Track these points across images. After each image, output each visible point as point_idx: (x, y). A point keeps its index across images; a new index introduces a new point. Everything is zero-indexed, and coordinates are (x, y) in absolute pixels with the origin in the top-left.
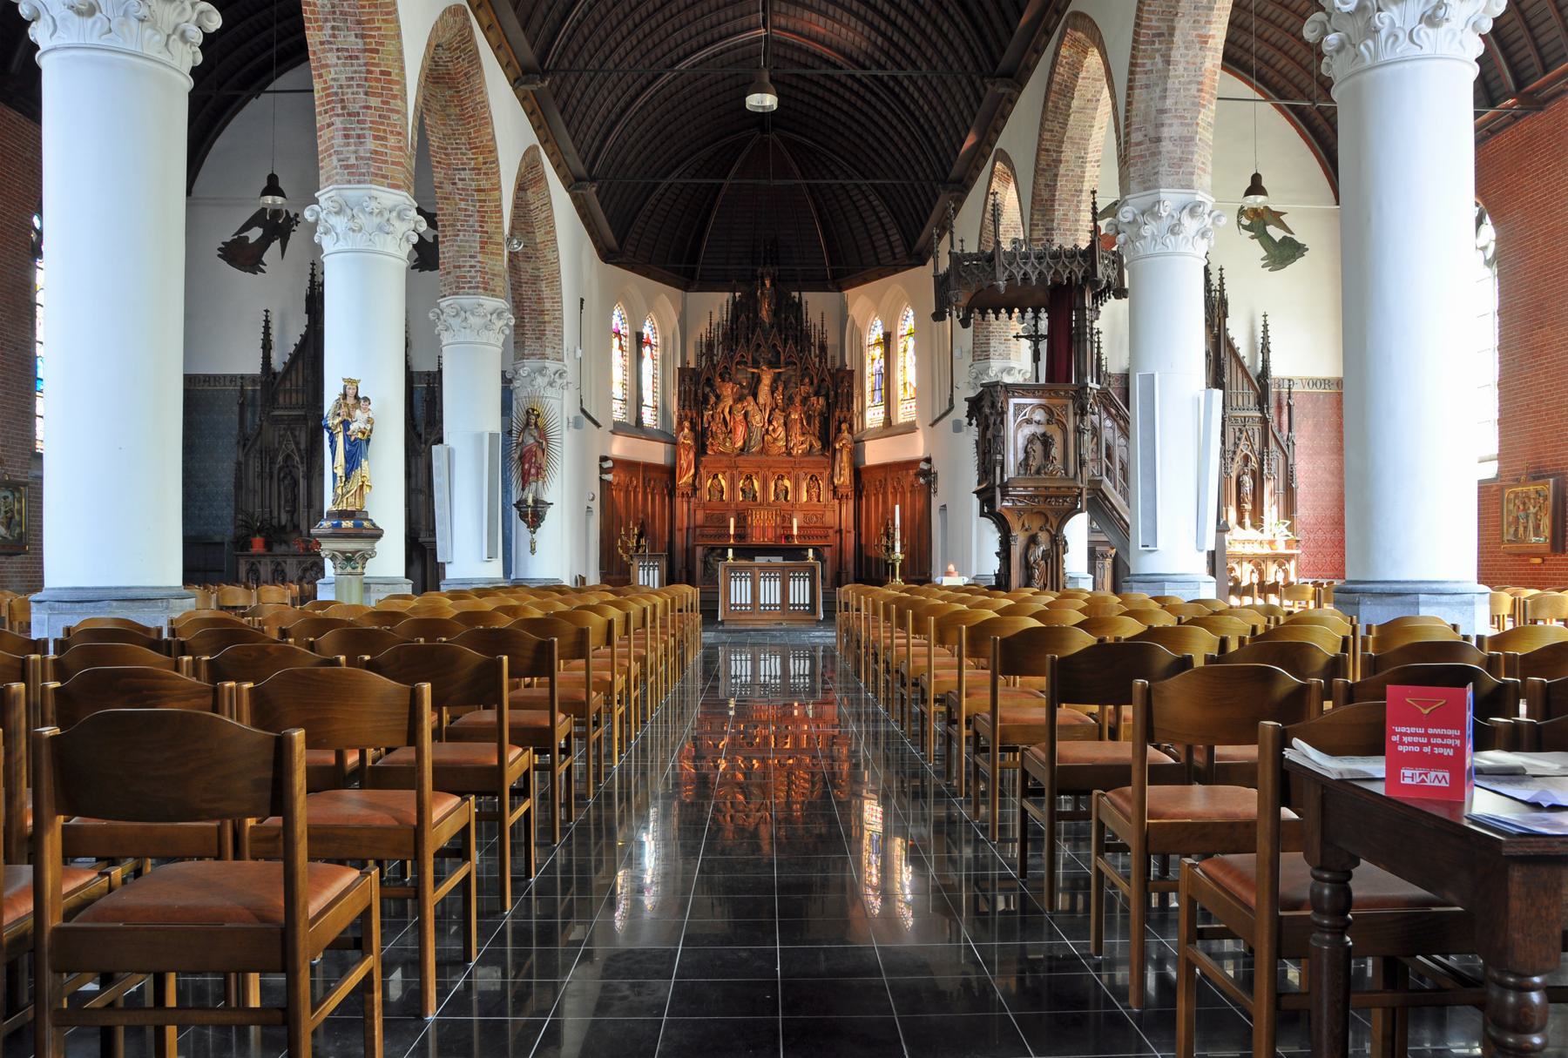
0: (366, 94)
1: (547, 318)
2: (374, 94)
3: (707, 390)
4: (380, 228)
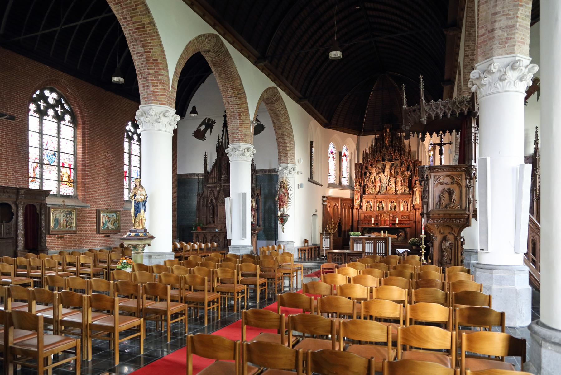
0: (148, 69)
1: (288, 149)
2: (151, 69)
3: (366, 171)
4: (156, 121)
